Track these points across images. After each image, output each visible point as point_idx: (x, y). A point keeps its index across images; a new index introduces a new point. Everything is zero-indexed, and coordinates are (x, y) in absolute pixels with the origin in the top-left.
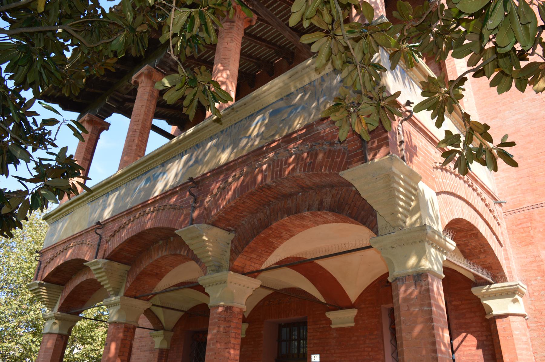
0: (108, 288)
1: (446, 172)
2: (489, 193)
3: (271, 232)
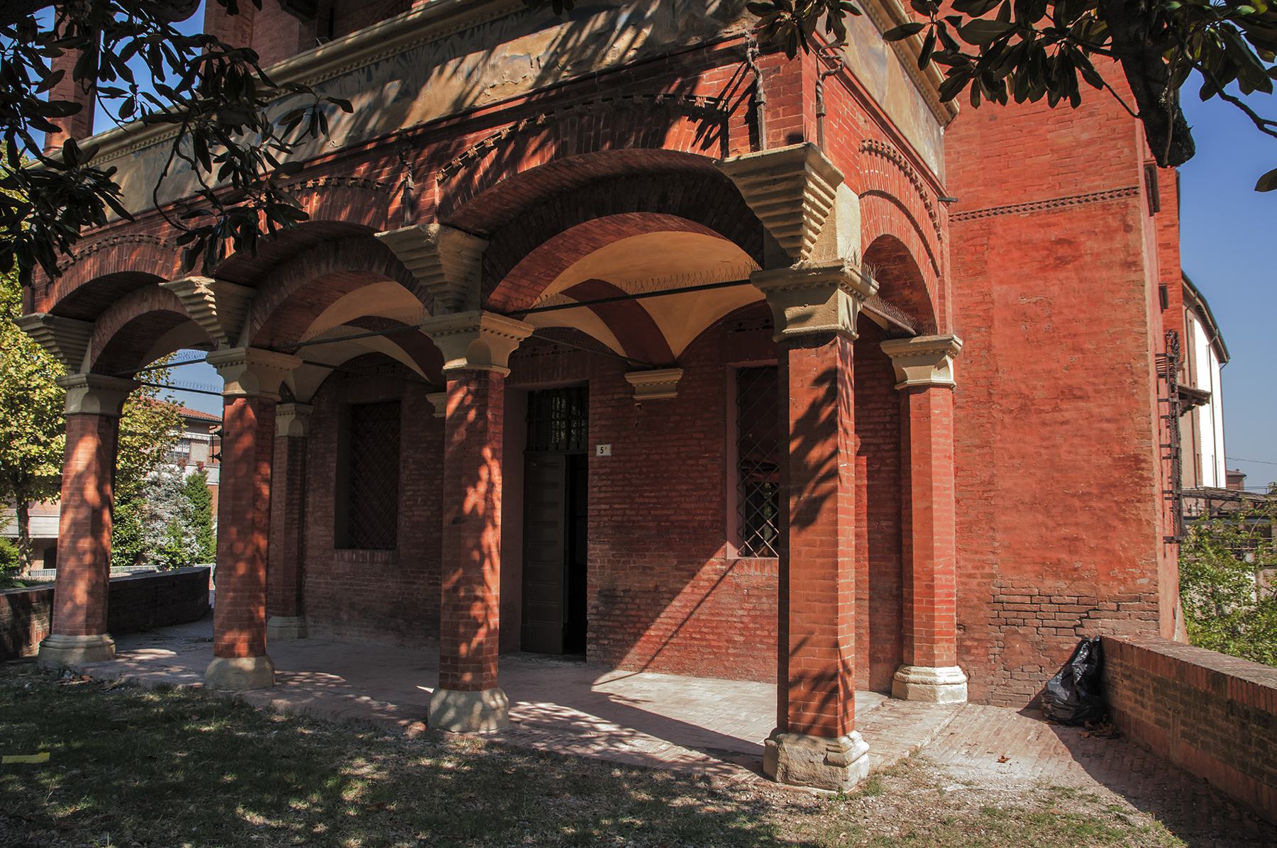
2: (932, 182)
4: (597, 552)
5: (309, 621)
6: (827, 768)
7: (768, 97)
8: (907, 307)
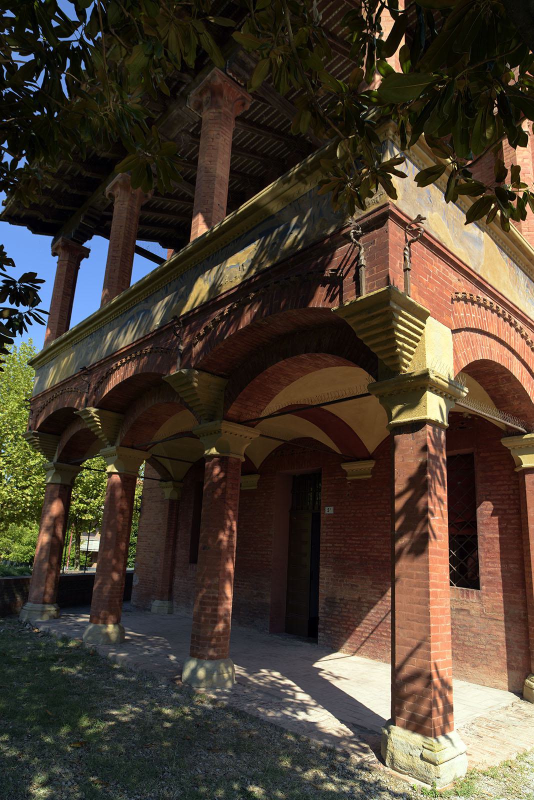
0: (103, 438)
1: (473, 304)
3: (266, 377)
4: (325, 573)
5: (175, 603)
6: (423, 763)
7: (367, 261)
8: (517, 415)
